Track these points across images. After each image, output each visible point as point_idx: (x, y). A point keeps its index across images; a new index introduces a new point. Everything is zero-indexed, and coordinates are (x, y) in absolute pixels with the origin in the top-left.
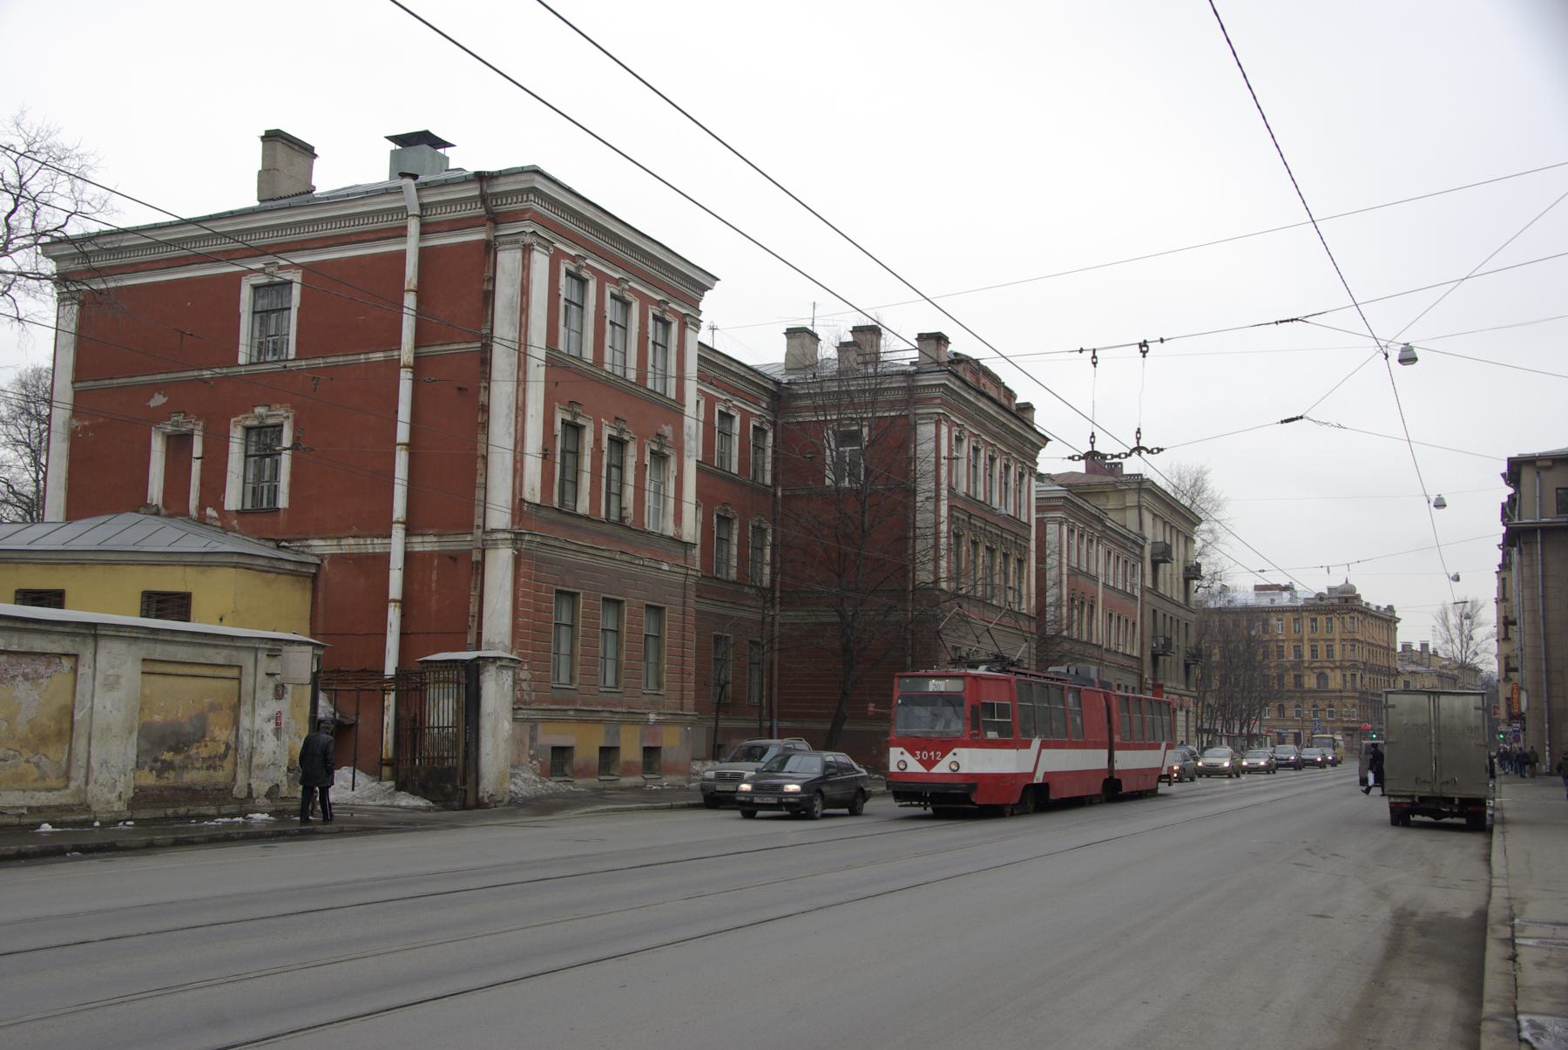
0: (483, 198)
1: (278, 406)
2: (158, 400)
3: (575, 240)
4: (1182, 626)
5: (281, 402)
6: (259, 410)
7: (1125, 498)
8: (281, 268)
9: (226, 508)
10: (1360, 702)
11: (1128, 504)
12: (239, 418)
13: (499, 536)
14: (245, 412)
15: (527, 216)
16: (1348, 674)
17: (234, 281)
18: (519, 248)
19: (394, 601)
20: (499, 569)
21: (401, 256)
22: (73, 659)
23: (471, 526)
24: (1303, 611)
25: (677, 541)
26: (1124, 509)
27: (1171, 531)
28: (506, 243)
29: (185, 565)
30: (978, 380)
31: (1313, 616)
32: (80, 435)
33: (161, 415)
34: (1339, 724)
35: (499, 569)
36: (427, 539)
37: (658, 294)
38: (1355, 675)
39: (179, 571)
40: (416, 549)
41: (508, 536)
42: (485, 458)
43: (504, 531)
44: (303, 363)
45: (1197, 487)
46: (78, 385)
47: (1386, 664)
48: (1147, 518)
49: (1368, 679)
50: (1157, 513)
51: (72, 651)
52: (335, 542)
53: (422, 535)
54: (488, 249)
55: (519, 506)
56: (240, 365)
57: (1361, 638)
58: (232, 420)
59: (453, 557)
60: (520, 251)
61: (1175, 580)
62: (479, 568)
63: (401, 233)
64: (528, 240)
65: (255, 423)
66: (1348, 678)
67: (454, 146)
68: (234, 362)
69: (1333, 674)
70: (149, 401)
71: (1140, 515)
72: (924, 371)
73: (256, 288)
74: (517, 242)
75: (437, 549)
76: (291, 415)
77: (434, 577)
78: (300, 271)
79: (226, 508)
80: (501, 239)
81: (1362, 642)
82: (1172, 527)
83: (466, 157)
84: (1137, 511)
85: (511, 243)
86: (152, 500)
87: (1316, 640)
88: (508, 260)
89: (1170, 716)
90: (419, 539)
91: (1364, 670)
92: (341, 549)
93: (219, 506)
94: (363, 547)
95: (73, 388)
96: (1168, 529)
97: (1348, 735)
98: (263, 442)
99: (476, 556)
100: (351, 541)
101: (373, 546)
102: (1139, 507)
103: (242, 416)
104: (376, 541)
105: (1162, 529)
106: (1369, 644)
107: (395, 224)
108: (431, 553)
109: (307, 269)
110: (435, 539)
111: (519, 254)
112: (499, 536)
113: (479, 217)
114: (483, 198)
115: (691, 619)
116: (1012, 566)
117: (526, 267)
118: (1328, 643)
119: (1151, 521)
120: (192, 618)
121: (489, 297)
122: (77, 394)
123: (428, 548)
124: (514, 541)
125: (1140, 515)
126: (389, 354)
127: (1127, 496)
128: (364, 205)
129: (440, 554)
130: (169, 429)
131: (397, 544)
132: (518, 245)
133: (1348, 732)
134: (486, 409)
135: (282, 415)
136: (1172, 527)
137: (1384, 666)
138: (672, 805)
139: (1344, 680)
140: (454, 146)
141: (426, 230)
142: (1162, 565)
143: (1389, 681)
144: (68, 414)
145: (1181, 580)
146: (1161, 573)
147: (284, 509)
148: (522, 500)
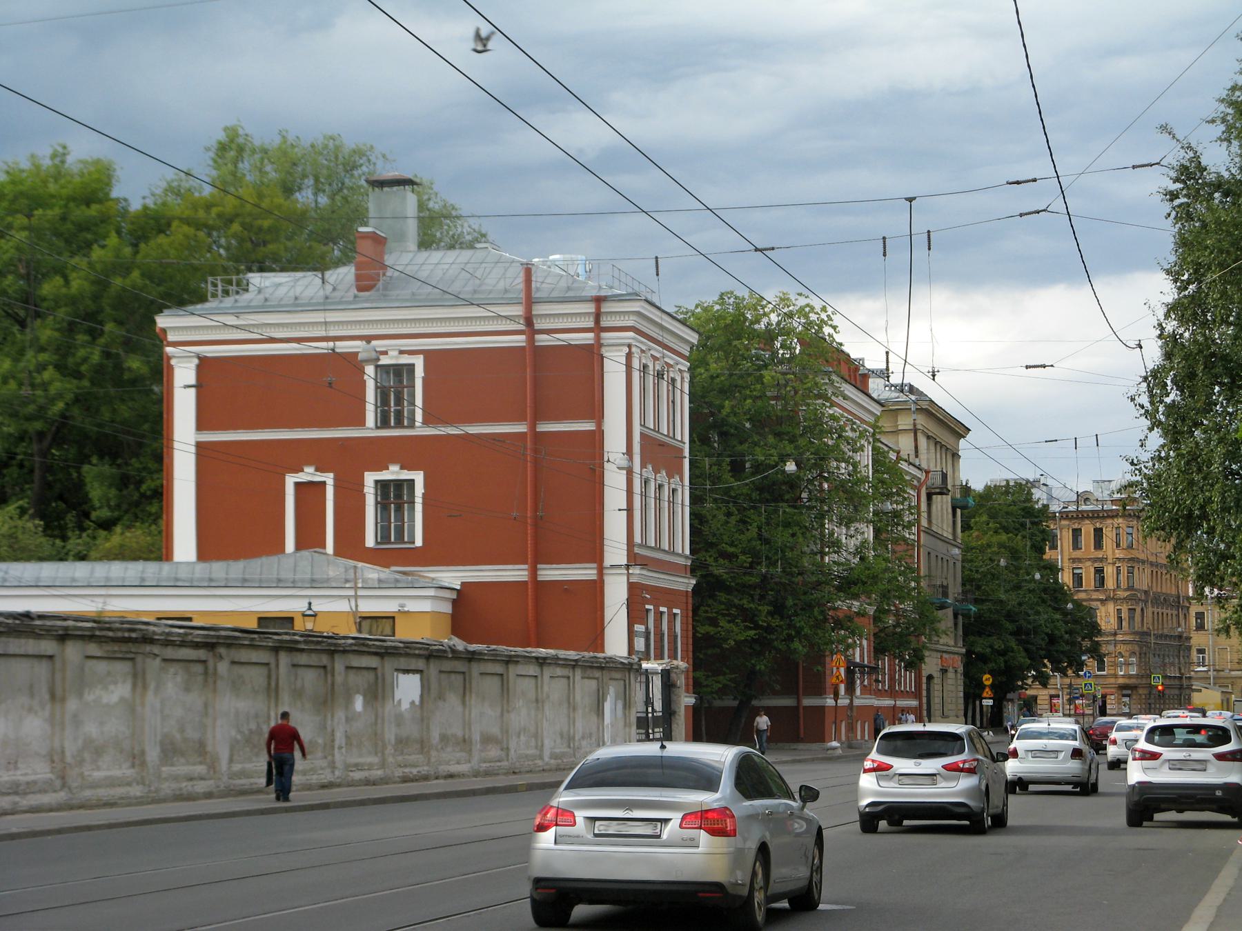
4: (951, 564)
7: (897, 416)
10: (1141, 648)
11: (900, 428)
16: (1125, 609)
19: (534, 572)
22: (391, 620)
24: (1062, 518)
26: (896, 432)
30: (237, 190)
31: (1076, 526)
34: (1112, 680)
38: (1135, 609)
45: (863, 359)
47: (1174, 592)
48: (923, 441)
49: (1150, 615)
57: (1142, 556)
66: (1125, 615)
68: (526, 433)
69: (1103, 609)
71: (916, 440)
81: (1143, 562)
82: (936, 443)
83: (843, 348)
87: (1079, 560)
91: (1146, 602)
96: (943, 450)
97: (1124, 696)
98: (394, 495)
102: (915, 431)
105: (934, 451)
106: (1152, 564)
109: (429, 355)
113: (870, 423)
118: (1096, 565)
120: (673, 738)
125: (916, 440)
127: (899, 418)
133: (1125, 692)
136: (936, 443)
137: (1172, 596)
138: (369, 342)
139: (1120, 619)
142: (934, 497)
143: (1178, 616)
145: (950, 510)
146: (934, 507)
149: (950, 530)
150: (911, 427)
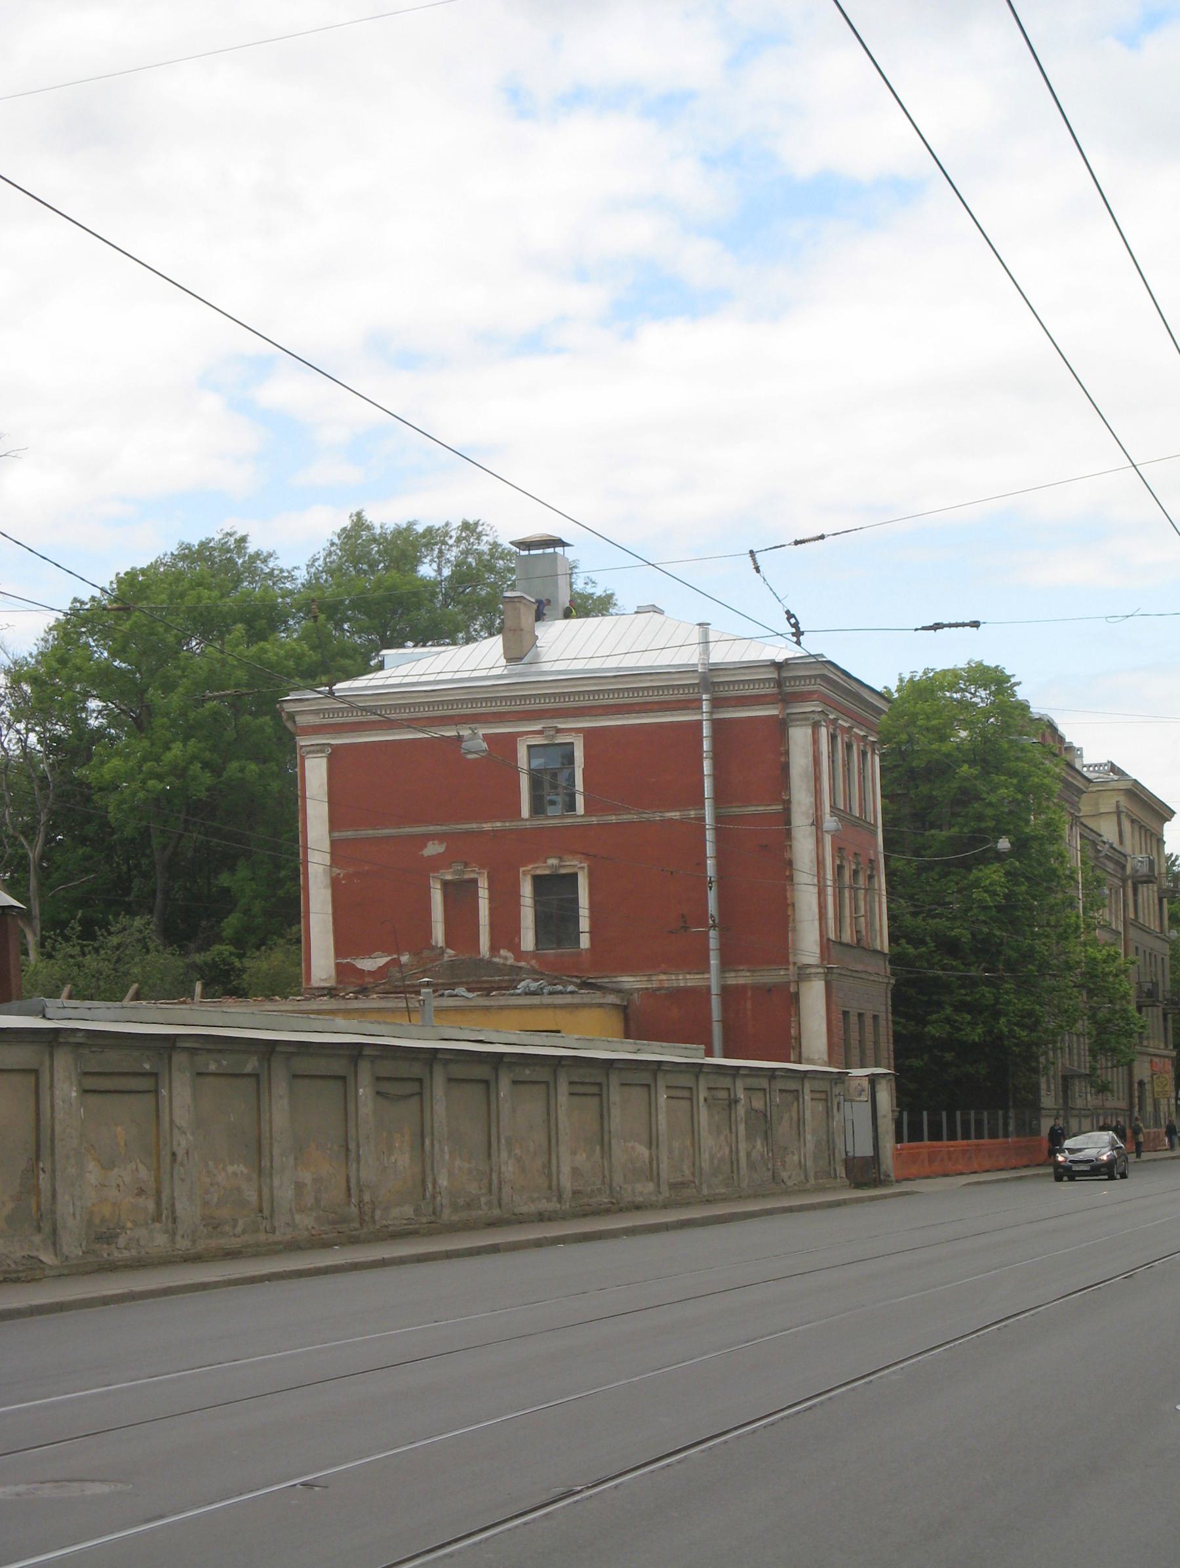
0: (779, 683)
1: (570, 857)
2: (433, 849)
3: (847, 713)
5: (574, 852)
6: (552, 861)
8: (558, 731)
9: (523, 949)
12: (529, 868)
13: (813, 970)
14: (535, 861)
15: (815, 696)
17: (512, 739)
18: (809, 725)
20: (814, 998)
21: (699, 723)
23: (787, 962)
25: (881, 953)
27: (1146, 833)
28: (798, 720)
29: (555, 1007)
32: (343, 882)
33: (436, 863)
35: (814, 998)
36: (742, 974)
37: (862, 730)
39: (550, 1013)
40: (729, 983)
41: (821, 970)
42: (793, 905)
43: (817, 966)
44: (594, 819)
46: (336, 834)
48: (1127, 826)
50: (1134, 817)
51: (598, 1081)
52: (645, 978)
53: (736, 971)
54: (780, 727)
55: (826, 945)
56: (523, 820)
58: (522, 869)
59: (769, 990)
60: (811, 727)
61: (1151, 902)
62: (794, 999)
63: (695, 705)
64: (817, 717)
65: (547, 872)
67: (572, 546)
70: (422, 849)
72: (1117, 792)
73: (529, 747)
74: (807, 719)
75: (750, 982)
76: (585, 865)
77: (749, 1005)
78: (582, 735)
79: (523, 949)
80: (794, 716)
82: (1141, 827)
84: (1116, 818)
85: (802, 720)
86: (437, 942)
88: (799, 737)
89: (650, 1148)
90: (733, 974)
92: (652, 984)
93: (515, 947)
94: (674, 982)
95: (330, 836)
99: (792, 989)
100: (663, 977)
101: (690, 980)
102: (1118, 813)
103: (532, 866)
104: (688, 976)
107: (692, 697)
108: (744, 987)
109: (590, 736)
110: (748, 974)
111: (810, 731)
112: (813, 970)
114: (779, 683)
115: (891, 1033)
116: (862, 881)
117: (816, 741)
119: (1130, 828)
121: (785, 768)
122: (334, 843)
123: (741, 981)
124: (826, 974)
126: (686, 813)
128: (651, 680)
129: (756, 988)
130: (449, 877)
131: (713, 979)
132: (808, 723)
134: (790, 863)
135: (576, 865)
136: (1141, 827)
140: (572, 546)
141: (717, 703)
144: (327, 859)
145: (1156, 901)
147: (586, 950)
148: (828, 940)
149: (1157, 923)
150: (1114, 810)
